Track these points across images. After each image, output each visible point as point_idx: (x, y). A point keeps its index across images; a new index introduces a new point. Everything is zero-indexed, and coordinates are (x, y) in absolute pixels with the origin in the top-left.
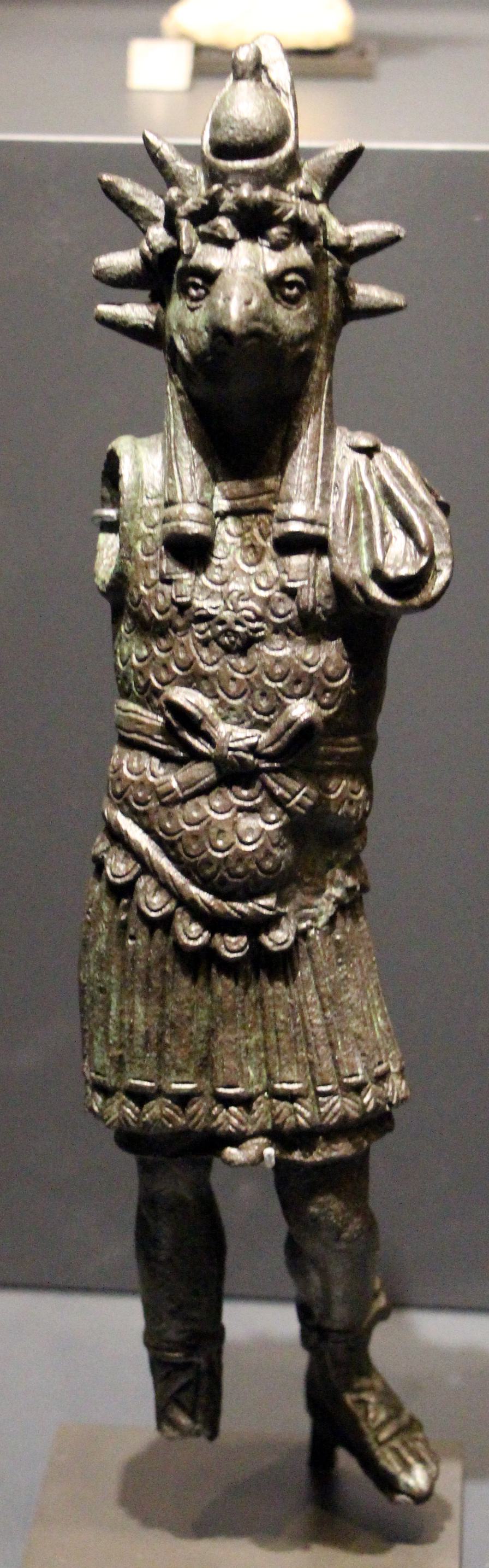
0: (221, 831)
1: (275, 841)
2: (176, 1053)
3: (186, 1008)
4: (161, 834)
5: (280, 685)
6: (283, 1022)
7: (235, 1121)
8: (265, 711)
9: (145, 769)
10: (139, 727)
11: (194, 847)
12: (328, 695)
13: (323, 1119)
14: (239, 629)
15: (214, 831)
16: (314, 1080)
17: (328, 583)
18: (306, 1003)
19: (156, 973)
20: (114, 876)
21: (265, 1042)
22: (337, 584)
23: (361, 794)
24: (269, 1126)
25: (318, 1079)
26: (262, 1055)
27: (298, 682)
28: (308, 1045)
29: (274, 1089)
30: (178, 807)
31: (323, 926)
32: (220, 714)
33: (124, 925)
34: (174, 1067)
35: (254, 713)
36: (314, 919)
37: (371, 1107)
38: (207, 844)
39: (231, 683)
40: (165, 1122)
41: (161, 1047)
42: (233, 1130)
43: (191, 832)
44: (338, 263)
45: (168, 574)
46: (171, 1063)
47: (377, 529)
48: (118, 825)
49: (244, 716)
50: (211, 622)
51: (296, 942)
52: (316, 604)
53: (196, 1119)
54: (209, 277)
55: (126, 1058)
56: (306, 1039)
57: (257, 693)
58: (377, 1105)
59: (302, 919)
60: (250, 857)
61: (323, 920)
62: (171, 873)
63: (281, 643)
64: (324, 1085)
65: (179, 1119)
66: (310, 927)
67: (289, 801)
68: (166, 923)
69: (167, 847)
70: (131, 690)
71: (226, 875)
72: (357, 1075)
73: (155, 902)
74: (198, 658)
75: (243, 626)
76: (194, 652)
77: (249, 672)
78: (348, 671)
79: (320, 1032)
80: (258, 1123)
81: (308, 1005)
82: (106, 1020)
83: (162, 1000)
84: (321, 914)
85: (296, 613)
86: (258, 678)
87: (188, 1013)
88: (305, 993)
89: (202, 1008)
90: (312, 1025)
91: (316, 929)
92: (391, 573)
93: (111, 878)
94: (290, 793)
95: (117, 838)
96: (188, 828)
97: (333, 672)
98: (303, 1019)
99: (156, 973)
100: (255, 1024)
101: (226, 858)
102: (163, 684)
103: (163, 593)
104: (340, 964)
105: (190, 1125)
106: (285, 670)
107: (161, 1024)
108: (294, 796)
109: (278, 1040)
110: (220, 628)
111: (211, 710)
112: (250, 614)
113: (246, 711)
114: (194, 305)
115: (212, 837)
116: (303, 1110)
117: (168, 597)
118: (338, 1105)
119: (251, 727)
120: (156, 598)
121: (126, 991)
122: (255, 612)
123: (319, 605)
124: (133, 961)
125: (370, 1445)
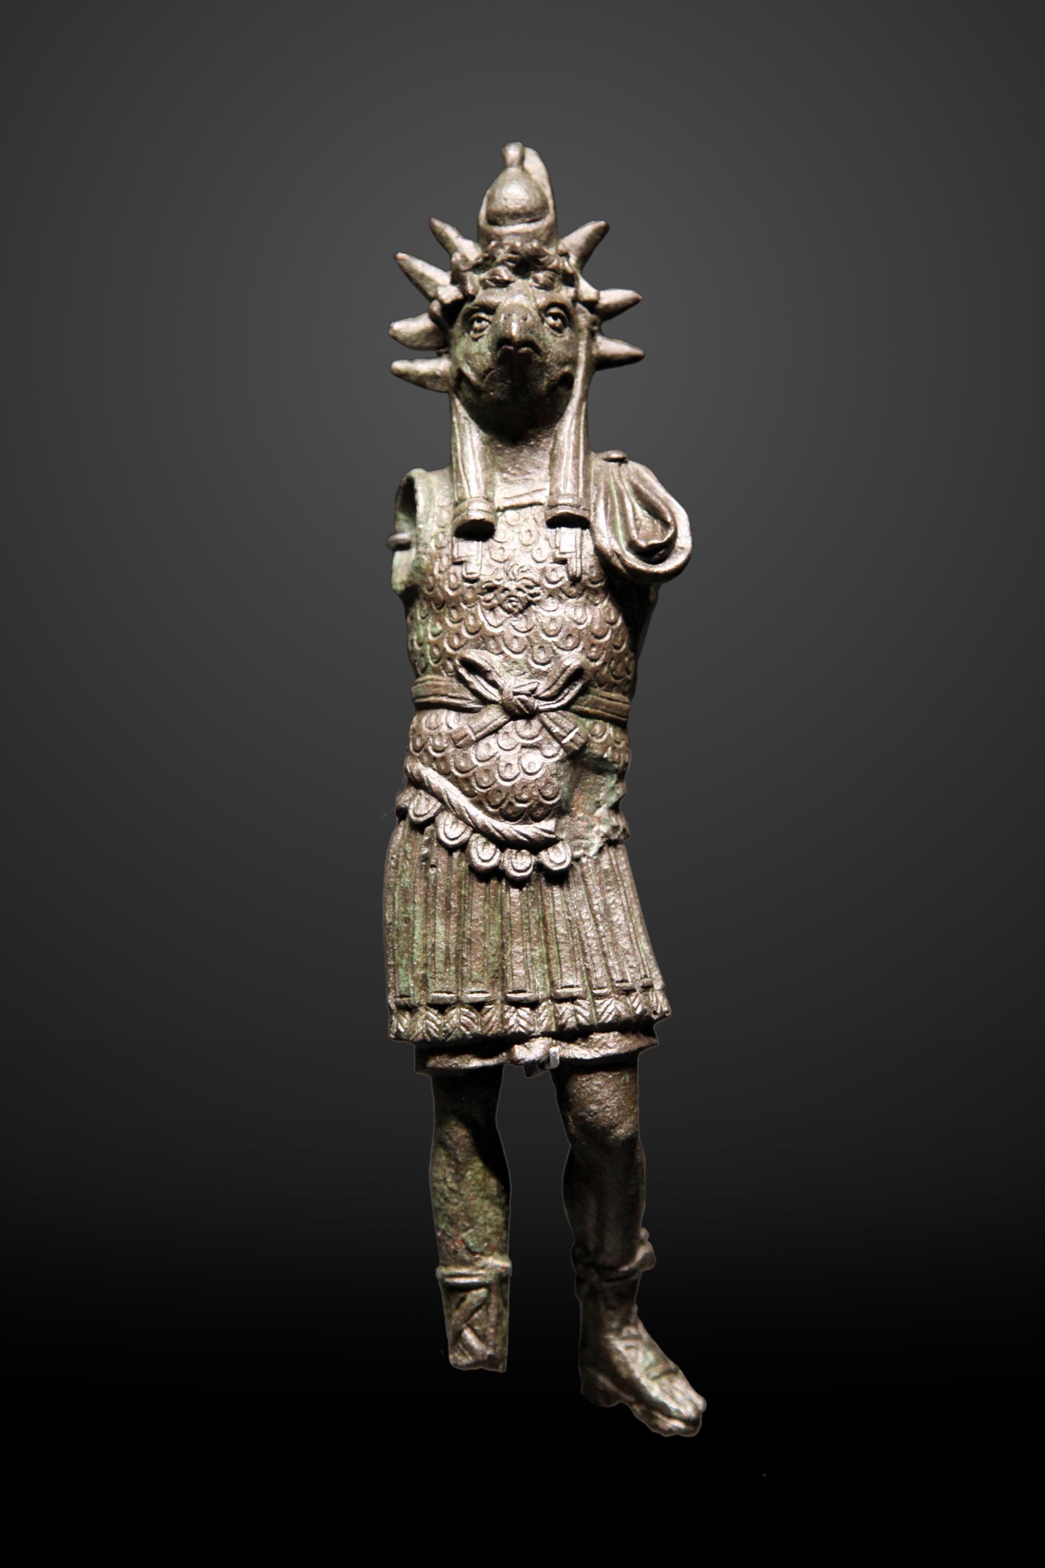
1: (554, 772)
2: (474, 967)
5: (555, 639)
6: (563, 935)
7: (523, 1023)
10: (435, 690)
11: (486, 780)
12: (594, 649)
13: (598, 1019)
14: (520, 594)
15: (503, 764)
16: (591, 985)
19: (454, 896)
20: (416, 815)
21: (548, 954)
22: (601, 556)
24: (553, 1029)
25: (594, 983)
26: (546, 966)
27: (570, 635)
28: (585, 954)
29: (556, 994)
30: (471, 749)
34: (470, 979)
35: (533, 664)
36: (586, 849)
37: (638, 1012)
38: (497, 776)
39: (515, 641)
40: (464, 1029)
41: (460, 961)
42: (523, 1030)
46: (469, 976)
48: (419, 773)
49: (526, 669)
50: (496, 592)
51: (571, 866)
52: (583, 573)
53: (490, 1025)
54: (490, 309)
55: (430, 975)
56: (583, 950)
57: (536, 647)
58: (644, 1011)
59: (578, 847)
61: (593, 851)
62: (462, 804)
64: (600, 988)
67: (564, 737)
70: (427, 664)
71: (513, 801)
72: (627, 981)
73: (450, 830)
74: (486, 623)
79: (594, 944)
80: (544, 1024)
81: (583, 921)
84: (592, 844)
85: (567, 579)
86: (537, 635)
87: (482, 929)
89: (495, 926)
90: (587, 938)
92: (643, 544)
93: (413, 818)
96: (480, 765)
98: (580, 932)
99: (454, 896)
100: (539, 939)
101: (513, 786)
102: (455, 649)
103: (455, 574)
106: (559, 626)
107: (458, 942)
109: (559, 951)
110: (503, 596)
113: (527, 663)
114: (478, 335)
115: (501, 769)
117: (459, 576)
119: (531, 678)
120: (449, 579)
121: (428, 916)
123: (585, 573)
124: (435, 888)
125: (638, 1380)
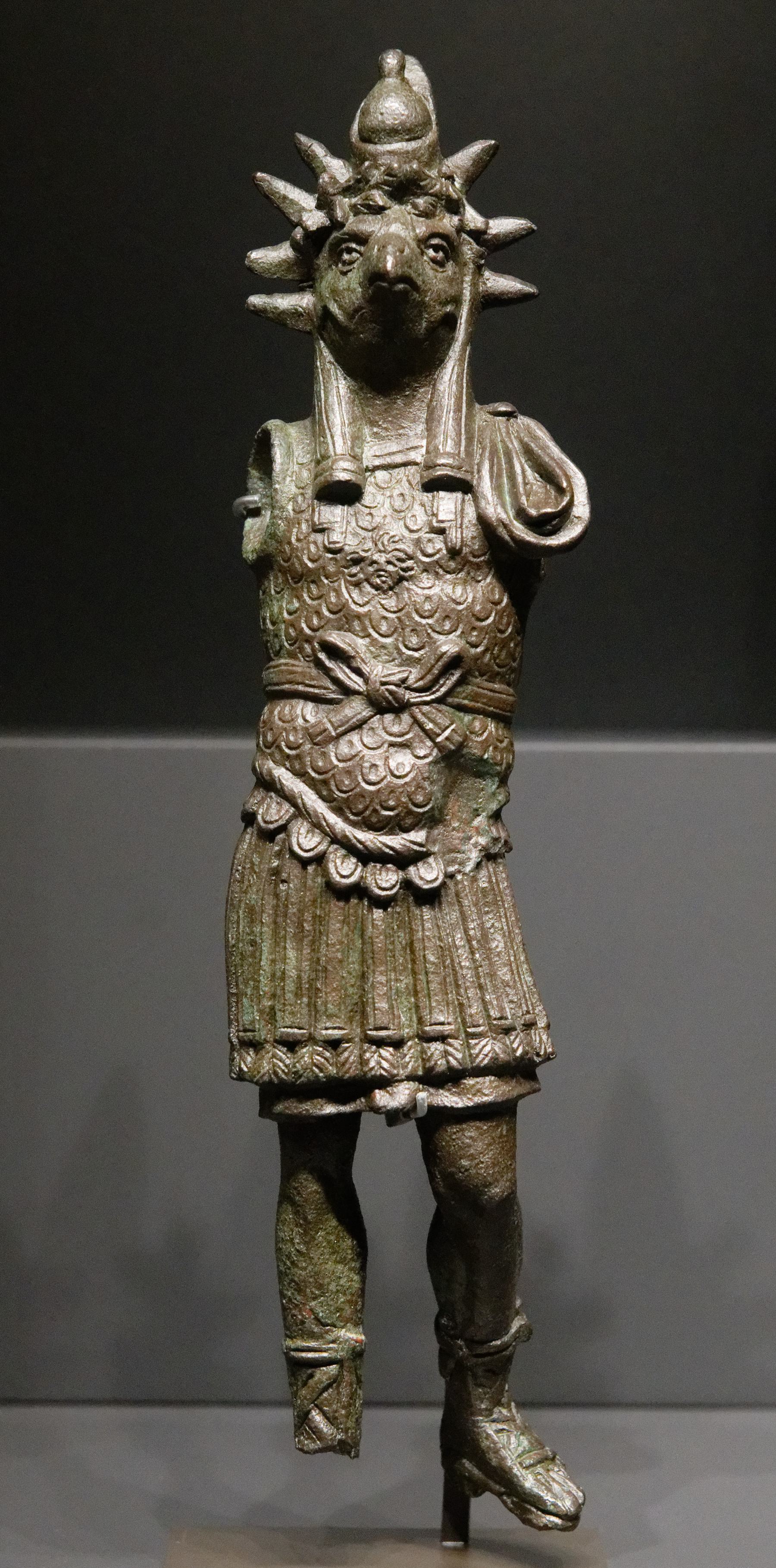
0: (374, 766)
1: (426, 775)
2: (330, 999)
3: (338, 950)
4: (313, 774)
5: (430, 621)
7: (385, 1065)
8: (415, 647)
9: (297, 716)
12: (475, 633)
14: (390, 568)
17: (475, 525)
18: (456, 946)
19: (308, 916)
20: (265, 822)
23: (504, 744)
24: (420, 1073)
25: (468, 1019)
29: (424, 1032)
31: (470, 871)
32: (371, 652)
33: (276, 872)
35: (404, 650)
36: (462, 864)
37: (519, 1053)
38: (360, 778)
43: (344, 768)
44: (475, 246)
45: (320, 524)
47: (520, 479)
49: (395, 655)
50: (362, 564)
51: (444, 884)
53: (347, 1066)
54: (362, 239)
55: (278, 1007)
58: (525, 1053)
60: (401, 790)
61: (468, 868)
63: (431, 582)
64: (474, 1026)
65: (330, 1068)
66: (459, 872)
68: (320, 859)
69: (319, 786)
70: (282, 647)
72: (506, 1019)
73: (305, 840)
75: (395, 566)
76: (347, 596)
77: (400, 610)
78: (493, 614)
79: (469, 974)
80: (410, 1066)
82: (257, 972)
83: (314, 945)
84: (469, 859)
88: (454, 936)
90: (461, 967)
91: (464, 874)
92: (533, 512)
93: (262, 824)
94: (440, 728)
95: (268, 785)
97: (480, 611)
98: (452, 961)
100: (405, 968)
101: (379, 791)
103: (315, 543)
104: (487, 913)
105: (340, 1074)
108: (443, 731)
109: (428, 982)
110: (371, 569)
111: (364, 649)
112: (402, 555)
113: (398, 649)
115: (365, 771)
116: (454, 1052)
117: (320, 545)
118: (488, 1048)
119: (401, 665)
122: (406, 554)
123: (466, 545)
125: (511, 1469)
